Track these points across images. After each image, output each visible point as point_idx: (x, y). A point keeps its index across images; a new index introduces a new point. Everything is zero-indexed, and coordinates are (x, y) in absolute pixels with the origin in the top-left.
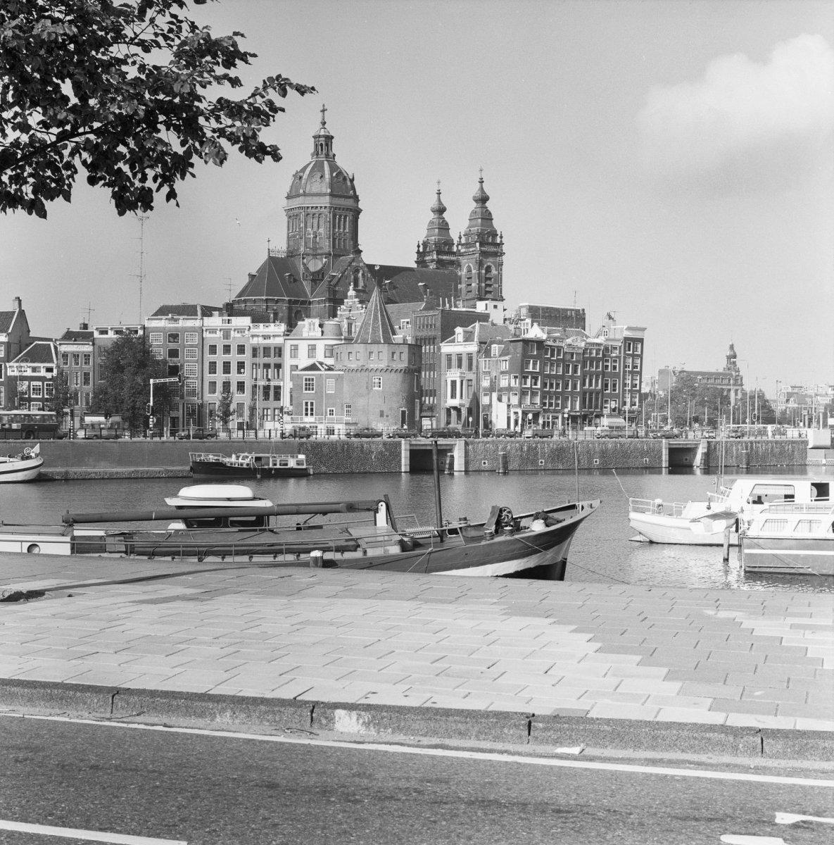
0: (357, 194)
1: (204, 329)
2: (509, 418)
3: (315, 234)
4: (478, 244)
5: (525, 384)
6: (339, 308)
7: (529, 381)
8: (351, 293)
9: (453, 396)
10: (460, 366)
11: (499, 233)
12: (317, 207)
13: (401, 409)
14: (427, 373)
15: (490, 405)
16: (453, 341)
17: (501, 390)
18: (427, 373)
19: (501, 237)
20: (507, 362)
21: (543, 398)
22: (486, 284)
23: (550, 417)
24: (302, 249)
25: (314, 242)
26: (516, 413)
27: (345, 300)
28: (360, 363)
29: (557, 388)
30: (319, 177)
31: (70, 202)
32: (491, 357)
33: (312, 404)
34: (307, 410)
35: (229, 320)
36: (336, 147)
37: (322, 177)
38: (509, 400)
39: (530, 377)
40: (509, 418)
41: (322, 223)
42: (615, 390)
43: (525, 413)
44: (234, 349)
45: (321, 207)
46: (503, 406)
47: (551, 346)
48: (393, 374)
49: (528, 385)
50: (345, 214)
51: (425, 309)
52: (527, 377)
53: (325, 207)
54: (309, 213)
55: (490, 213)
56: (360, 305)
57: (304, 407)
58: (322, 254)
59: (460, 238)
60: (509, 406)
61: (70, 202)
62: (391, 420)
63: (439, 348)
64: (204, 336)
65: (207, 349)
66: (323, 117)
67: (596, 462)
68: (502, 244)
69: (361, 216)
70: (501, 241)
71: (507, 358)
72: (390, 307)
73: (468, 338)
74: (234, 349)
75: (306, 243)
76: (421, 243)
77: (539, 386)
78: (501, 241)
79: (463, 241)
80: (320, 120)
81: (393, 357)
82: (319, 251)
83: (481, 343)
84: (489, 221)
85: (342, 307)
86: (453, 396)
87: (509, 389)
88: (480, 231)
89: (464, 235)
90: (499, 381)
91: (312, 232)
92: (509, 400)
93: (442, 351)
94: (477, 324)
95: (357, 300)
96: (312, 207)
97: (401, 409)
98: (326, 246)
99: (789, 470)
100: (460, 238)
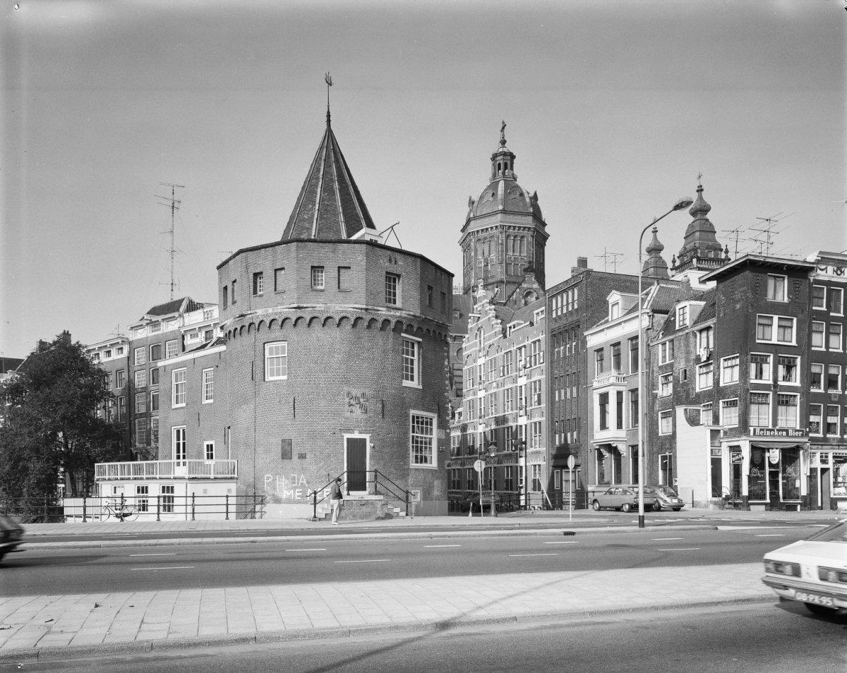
2: (716, 463)
3: (486, 260)
5: (760, 374)
7: (768, 369)
9: (603, 426)
10: (618, 366)
12: (487, 229)
13: (347, 436)
14: (568, 390)
15: (674, 436)
17: (698, 399)
18: (568, 390)
19: (727, 252)
20: (711, 333)
21: (808, 410)
23: (831, 460)
25: (486, 271)
26: (736, 449)
30: (491, 195)
32: (675, 332)
36: (518, 168)
37: (493, 194)
38: (716, 420)
39: (771, 359)
40: (716, 463)
41: (493, 248)
43: (758, 451)
45: (492, 228)
46: (703, 433)
47: (828, 283)
49: (768, 378)
50: (521, 235)
52: (764, 360)
53: (496, 227)
54: (483, 237)
55: (711, 225)
57: (174, 442)
58: (493, 283)
59: (674, 262)
60: (714, 434)
62: (313, 468)
63: (584, 342)
66: (503, 135)
70: (727, 256)
71: (710, 323)
75: (476, 274)
77: (796, 381)
78: (727, 256)
80: (499, 138)
81: (314, 281)
82: (490, 281)
83: (655, 311)
84: (710, 234)
86: (603, 426)
87: (717, 393)
89: (678, 257)
90: (693, 381)
91: (483, 260)
92: (716, 420)
93: (589, 345)
96: (482, 230)
97: (347, 436)
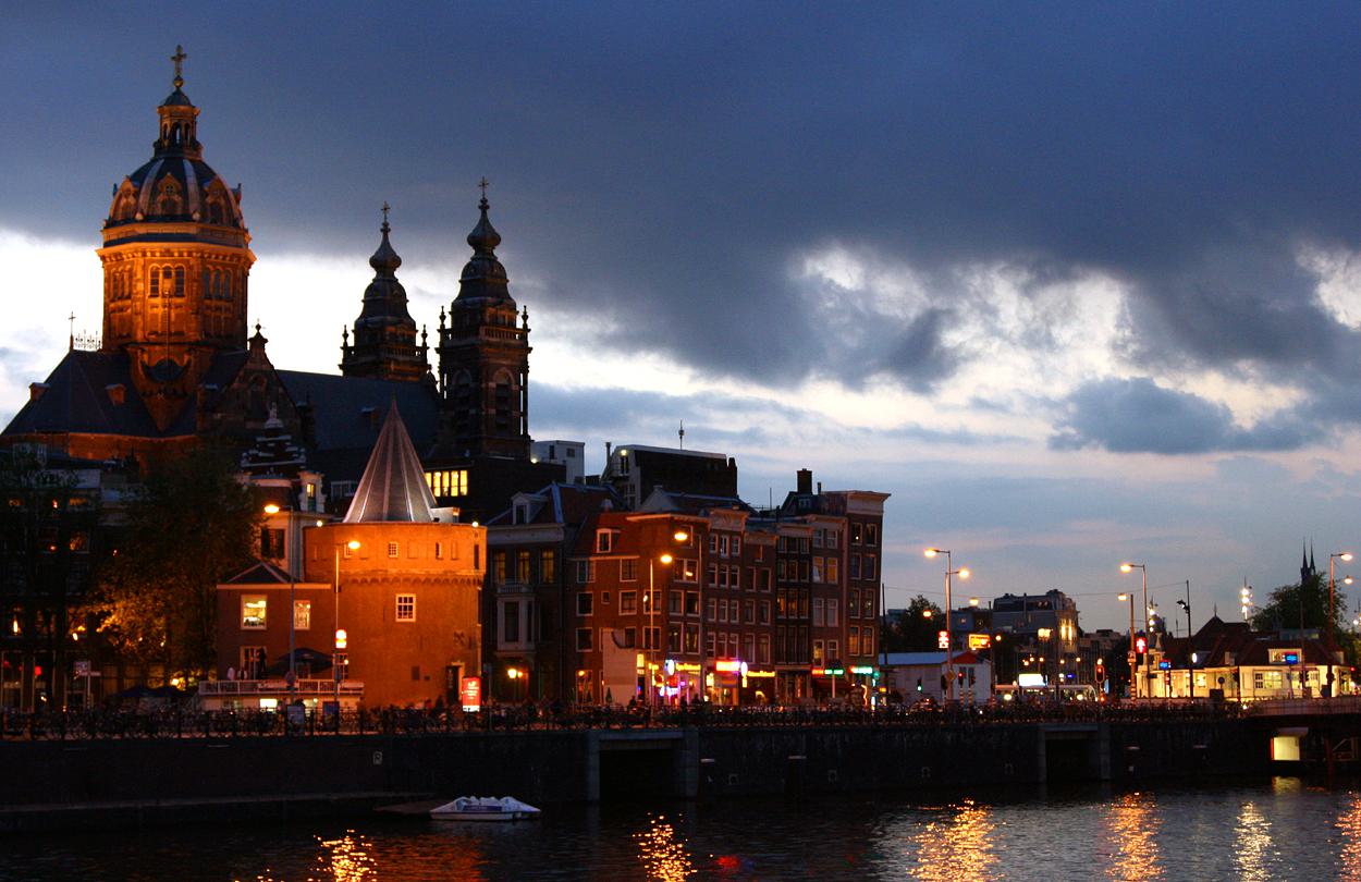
31: (887, 496)
61: (887, 496)
70: (525, 325)
76: (351, 327)
78: (525, 325)
80: (172, 74)
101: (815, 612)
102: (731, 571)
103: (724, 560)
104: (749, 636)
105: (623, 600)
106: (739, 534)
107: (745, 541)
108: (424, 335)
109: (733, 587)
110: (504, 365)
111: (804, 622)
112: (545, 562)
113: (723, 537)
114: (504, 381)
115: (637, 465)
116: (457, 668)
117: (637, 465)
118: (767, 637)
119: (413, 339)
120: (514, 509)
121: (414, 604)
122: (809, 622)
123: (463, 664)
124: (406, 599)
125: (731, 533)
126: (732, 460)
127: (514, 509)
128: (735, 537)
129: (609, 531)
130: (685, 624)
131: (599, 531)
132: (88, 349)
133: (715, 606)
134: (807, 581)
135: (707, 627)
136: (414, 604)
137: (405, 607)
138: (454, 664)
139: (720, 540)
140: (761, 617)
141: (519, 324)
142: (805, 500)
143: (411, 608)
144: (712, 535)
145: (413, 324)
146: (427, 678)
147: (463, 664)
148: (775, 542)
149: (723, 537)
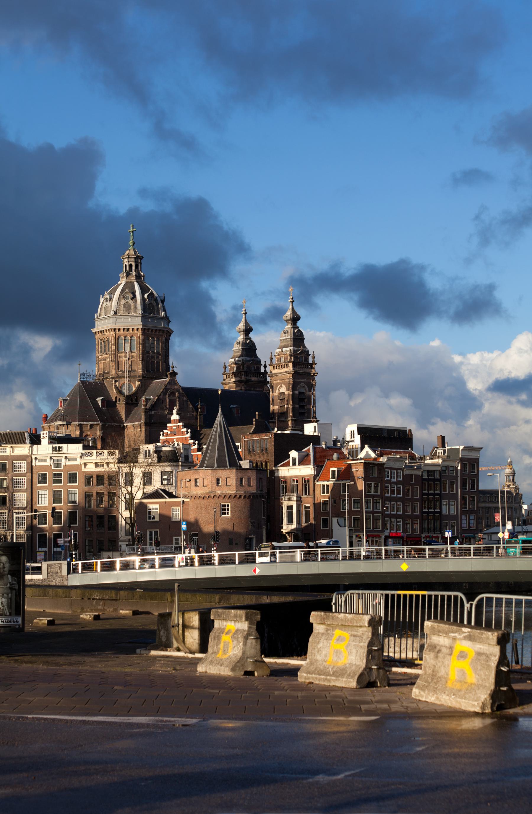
0: (168, 315)
1: (34, 457)
4: (291, 365)
6: (161, 433)
8: (175, 417)
11: (311, 353)
16: (287, 465)
19: (314, 357)
22: (300, 406)
24: (113, 372)
27: (169, 425)
28: (207, 490)
29: (397, 511)
33: (156, 533)
34: (151, 539)
35: (59, 447)
42: (453, 491)
44: (64, 477)
45: (133, 329)
48: (201, 499)
51: (255, 432)
53: (137, 329)
56: (185, 430)
61: (481, 448)
64: (33, 464)
65: (36, 479)
67: (465, 586)
68: (314, 363)
69: (172, 337)
70: (314, 361)
72: (232, 428)
73: (303, 461)
74: (64, 477)
78: (314, 361)
79: (275, 361)
85: (165, 431)
88: (292, 351)
94: (311, 447)
95: (181, 424)
98: (139, 369)
99: (89, 568)
100: (272, 358)
101: (444, 507)
102: (397, 488)
103: (394, 483)
104: (415, 521)
105: (354, 502)
106: (401, 469)
107: (404, 473)
108: (265, 367)
109: (392, 495)
110: (303, 382)
111: (437, 512)
112: (40, 496)
113: (393, 471)
114: (302, 390)
115: (358, 434)
116: (251, 539)
117: (358, 434)
118: (417, 521)
119: (259, 369)
120: (291, 459)
121: (229, 508)
122: (440, 512)
123: (255, 537)
124: (225, 505)
125: (397, 469)
126: (410, 431)
127: (291, 459)
128: (399, 471)
129: (335, 469)
130: (373, 514)
131: (331, 469)
132: (141, 366)
133: (395, 506)
134: (439, 492)
135: (385, 516)
136: (229, 508)
137: (225, 509)
138: (250, 537)
139: (391, 473)
140: (413, 510)
141: (311, 361)
142: (440, 451)
143: (228, 510)
144: (387, 470)
145: (308, 351)
146: (236, 544)
147: (255, 537)
148: (421, 474)
149: (393, 471)
